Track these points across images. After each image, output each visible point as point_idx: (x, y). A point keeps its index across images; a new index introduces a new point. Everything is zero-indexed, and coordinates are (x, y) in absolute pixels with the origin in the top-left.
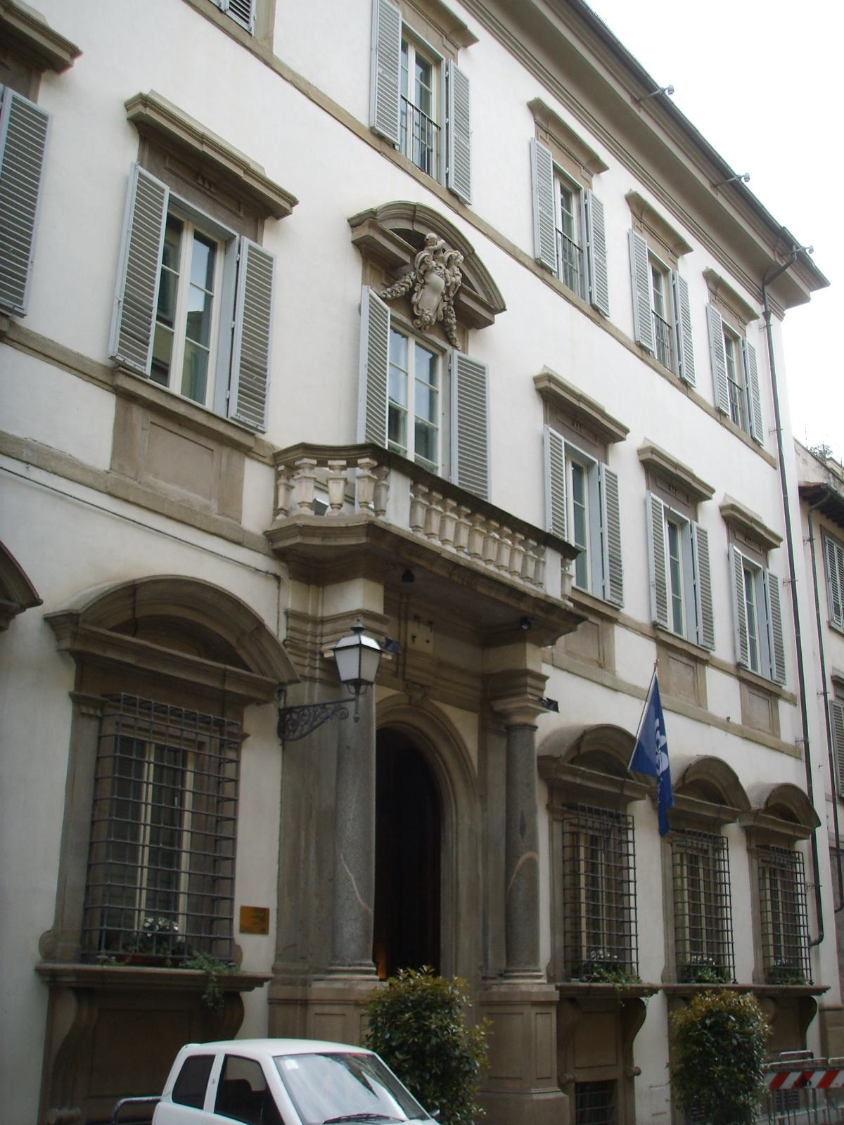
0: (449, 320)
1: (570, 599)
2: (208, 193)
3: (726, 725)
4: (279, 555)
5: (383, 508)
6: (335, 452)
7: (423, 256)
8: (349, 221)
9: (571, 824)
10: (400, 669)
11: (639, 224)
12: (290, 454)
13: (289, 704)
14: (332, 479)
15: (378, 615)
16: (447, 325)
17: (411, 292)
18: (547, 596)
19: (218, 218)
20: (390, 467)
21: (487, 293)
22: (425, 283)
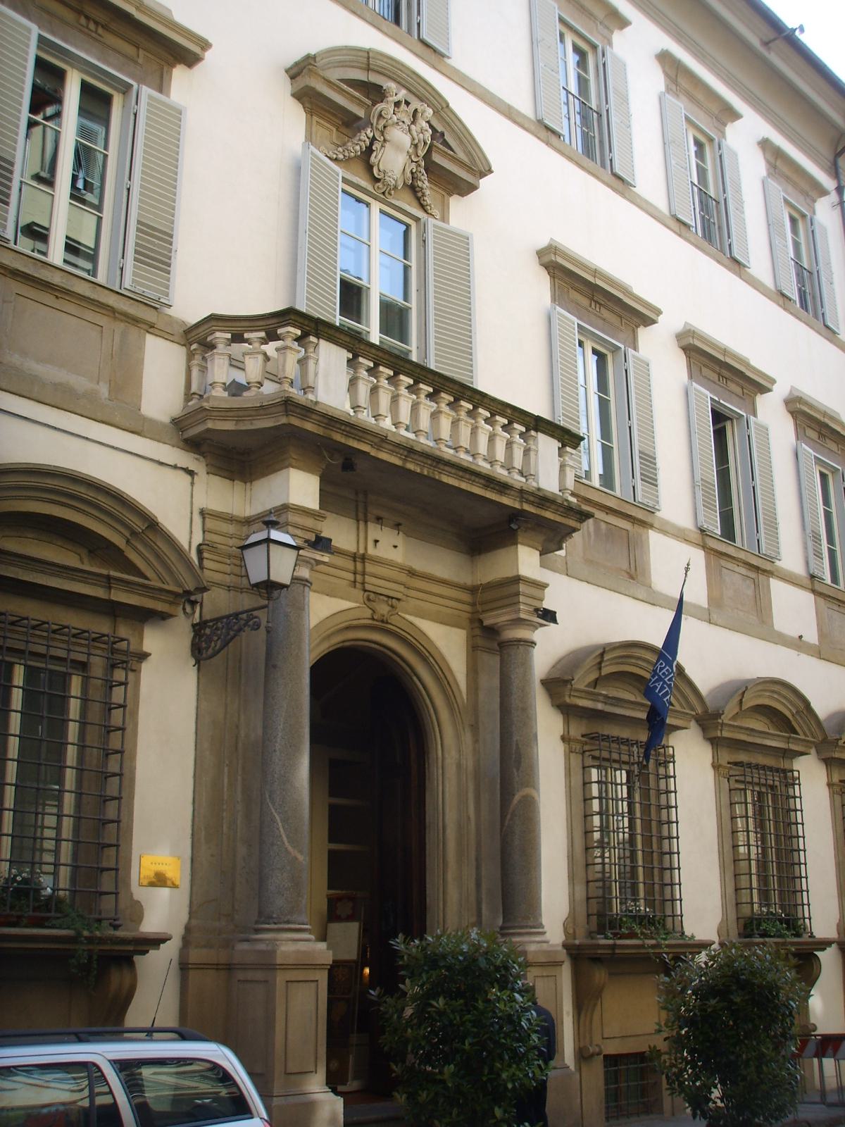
0: (420, 184)
1: (573, 494)
2: (94, 35)
3: (798, 644)
4: (194, 445)
5: (311, 384)
6: (253, 321)
7: (379, 108)
8: (287, 71)
9: (594, 758)
10: (359, 578)
11: (674, 88)
12: (201, 329)
13: (207, 617)
14: (248, 354)
15: (313, 510)
16: (418, 189)
17: (369, 150)
18: (539, 489)
19: (109, 64)
20: (537, 430)
21: (469, 154)
22: (385, 141)
